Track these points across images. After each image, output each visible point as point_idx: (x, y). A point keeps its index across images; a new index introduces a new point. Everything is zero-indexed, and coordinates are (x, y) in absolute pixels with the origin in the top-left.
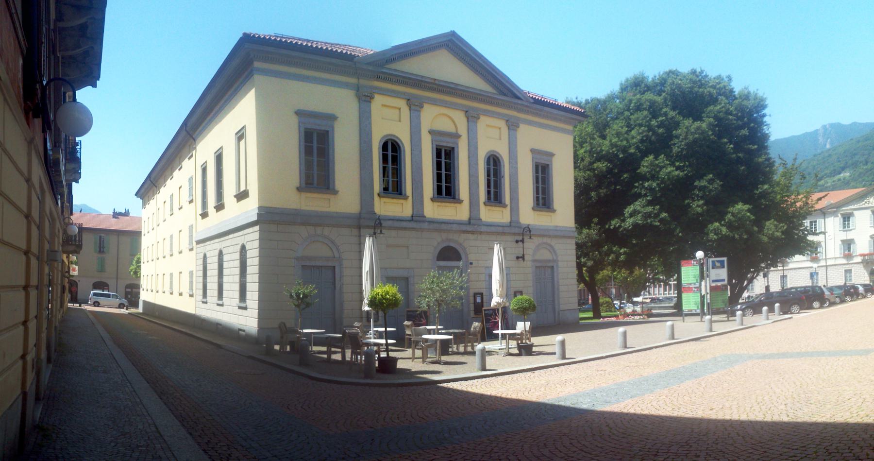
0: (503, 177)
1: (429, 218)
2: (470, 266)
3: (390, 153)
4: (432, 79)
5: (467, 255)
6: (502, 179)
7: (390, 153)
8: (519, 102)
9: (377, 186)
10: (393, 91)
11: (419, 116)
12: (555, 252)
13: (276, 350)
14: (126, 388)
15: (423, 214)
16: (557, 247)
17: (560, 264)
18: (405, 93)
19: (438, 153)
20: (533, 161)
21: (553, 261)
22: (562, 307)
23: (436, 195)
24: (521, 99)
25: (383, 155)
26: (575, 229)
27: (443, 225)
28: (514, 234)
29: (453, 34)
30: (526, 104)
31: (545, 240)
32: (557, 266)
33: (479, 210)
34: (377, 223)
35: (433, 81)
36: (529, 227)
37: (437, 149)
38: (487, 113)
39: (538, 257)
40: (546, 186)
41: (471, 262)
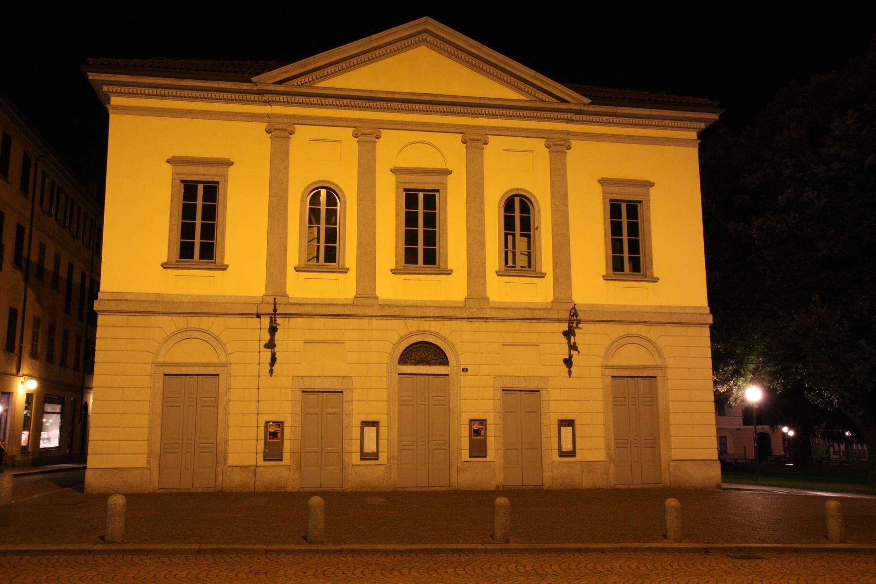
0: (537, 229)
1: (383, 300)
3: (517, 214)
4: (387, 92)
5: (457, 356)
6: (537, 232)
7: (517, 214)
8: (563, 106)
9: (294, 255)
10: (423, 124)
11: (374, 149)
12: (659, 351)
13: (847, 431)
14: (553, 465)
15: (285, 293)
16: (661, 343)
17: (670, 373)
18: (347, 120)
19: (411, 199)
20: (604, 198)
21: (656, 367)
22: (676, 454)
24: (563, 101)
25: (407, 232)
26: (708, 310)
27: (408, 309)
28: (559, 320)
30: (577, 107)
31: (634, 329)
32: (665, 376)
33: (484, 285)
34: (572, 314)
35: (389, 96)
36: (576, 308)
37: (612, 206)
38: (501, 132)
39: (616, 361)
40: (216, 222)
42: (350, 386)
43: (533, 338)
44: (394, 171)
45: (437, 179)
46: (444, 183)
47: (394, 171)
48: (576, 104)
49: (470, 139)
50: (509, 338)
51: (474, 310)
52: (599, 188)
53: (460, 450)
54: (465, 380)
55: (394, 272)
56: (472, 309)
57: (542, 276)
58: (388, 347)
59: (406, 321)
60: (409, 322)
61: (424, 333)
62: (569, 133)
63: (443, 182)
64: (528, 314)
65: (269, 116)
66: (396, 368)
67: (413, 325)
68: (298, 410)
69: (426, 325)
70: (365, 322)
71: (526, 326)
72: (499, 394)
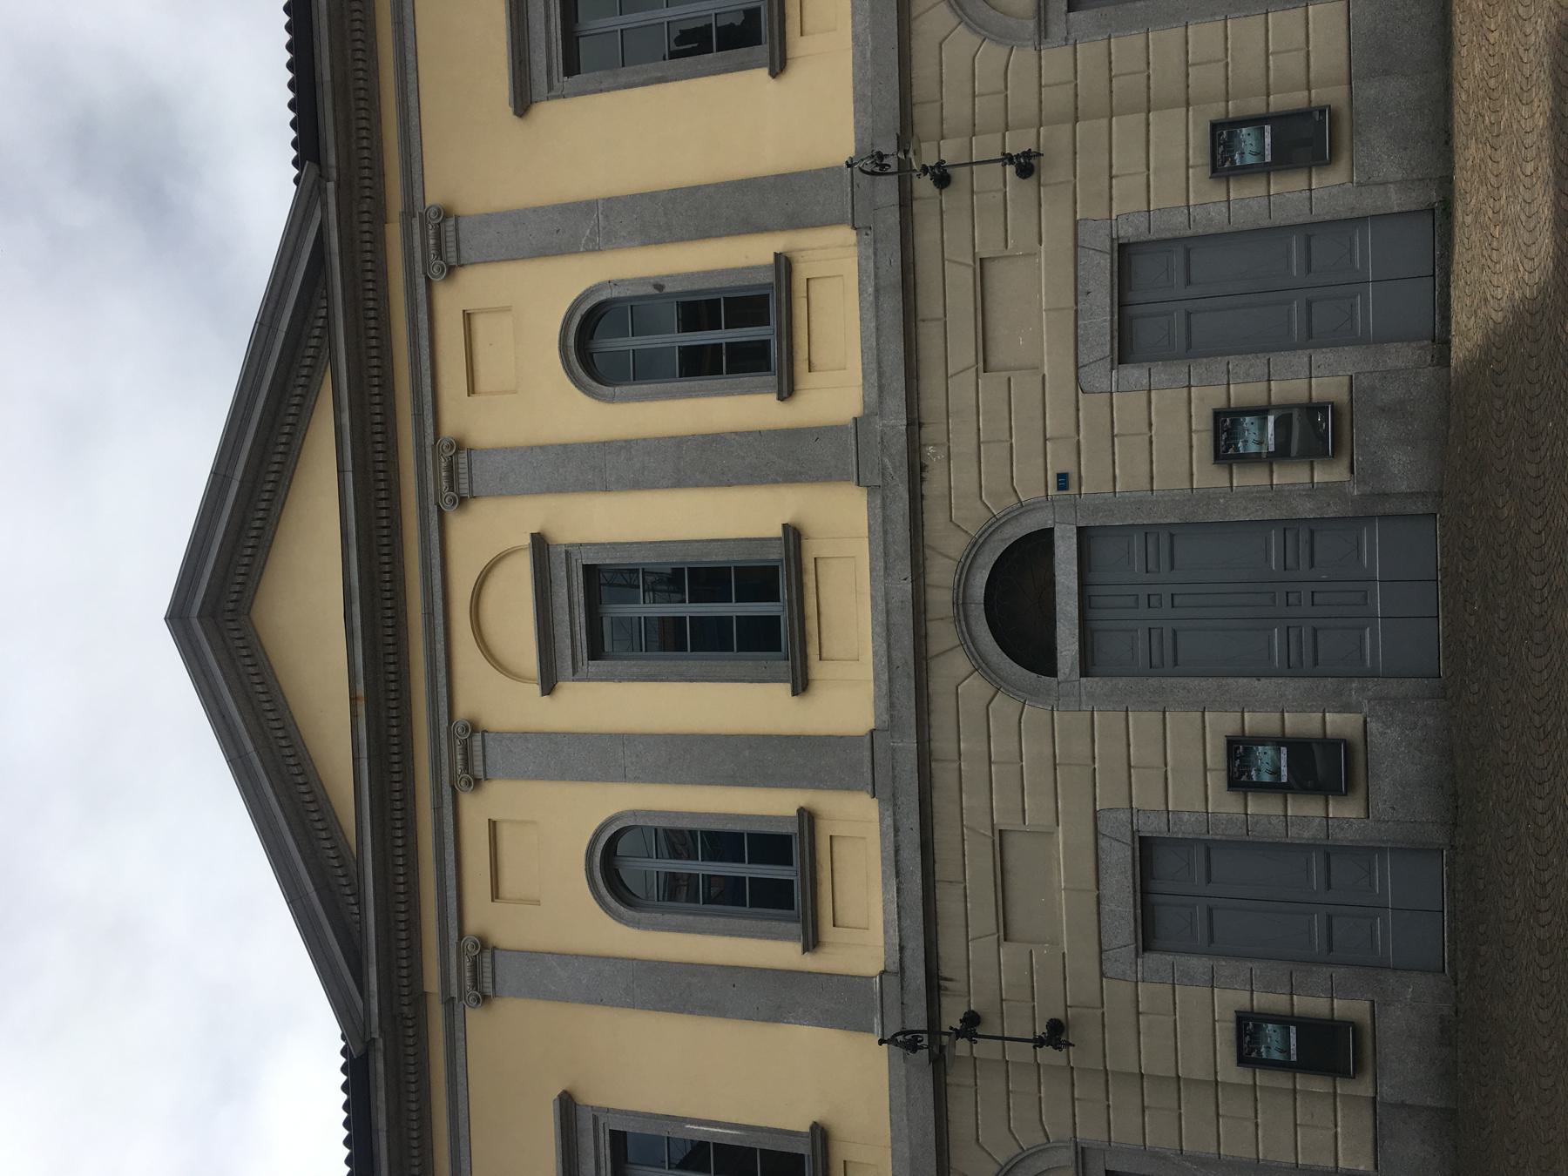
0: (659, 287)
2: (1073, 490)
5: (1023, 509)
9: (782, 953)
10: (429, 614)
18: (438, 809)
23: (762, 51)
29: (177, 618)
41: (1052, 480)
42: (1125, 817)
43: (961, 280)
44: (548, 686)
45: (559, 573)
46: (567, 552)
47: (548, 686)
48: (325, 205)
49: (451, 489)
50: (963, 352)
51: (886, 460)
52: (548, 112)
53: (1313, 490)
54: (1092, 482)
55: (801, 684)
56: (884, 468)
57: (784, 265)
58: (1004, 706)
59: (931, 654)
60: (934, 647)
61: (961, 603)
62: (408, 214)
63: (563, 556)
64: (893, 302)
65: (449, 1002)
66: (1066, 681)
67: (943, 635)
68: (1198, 964)
69: (940, 599)
70: (944, 776)
71: (929, 305)
72: (1134, 373)
